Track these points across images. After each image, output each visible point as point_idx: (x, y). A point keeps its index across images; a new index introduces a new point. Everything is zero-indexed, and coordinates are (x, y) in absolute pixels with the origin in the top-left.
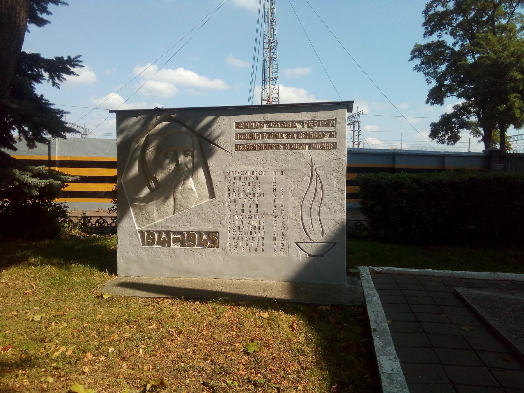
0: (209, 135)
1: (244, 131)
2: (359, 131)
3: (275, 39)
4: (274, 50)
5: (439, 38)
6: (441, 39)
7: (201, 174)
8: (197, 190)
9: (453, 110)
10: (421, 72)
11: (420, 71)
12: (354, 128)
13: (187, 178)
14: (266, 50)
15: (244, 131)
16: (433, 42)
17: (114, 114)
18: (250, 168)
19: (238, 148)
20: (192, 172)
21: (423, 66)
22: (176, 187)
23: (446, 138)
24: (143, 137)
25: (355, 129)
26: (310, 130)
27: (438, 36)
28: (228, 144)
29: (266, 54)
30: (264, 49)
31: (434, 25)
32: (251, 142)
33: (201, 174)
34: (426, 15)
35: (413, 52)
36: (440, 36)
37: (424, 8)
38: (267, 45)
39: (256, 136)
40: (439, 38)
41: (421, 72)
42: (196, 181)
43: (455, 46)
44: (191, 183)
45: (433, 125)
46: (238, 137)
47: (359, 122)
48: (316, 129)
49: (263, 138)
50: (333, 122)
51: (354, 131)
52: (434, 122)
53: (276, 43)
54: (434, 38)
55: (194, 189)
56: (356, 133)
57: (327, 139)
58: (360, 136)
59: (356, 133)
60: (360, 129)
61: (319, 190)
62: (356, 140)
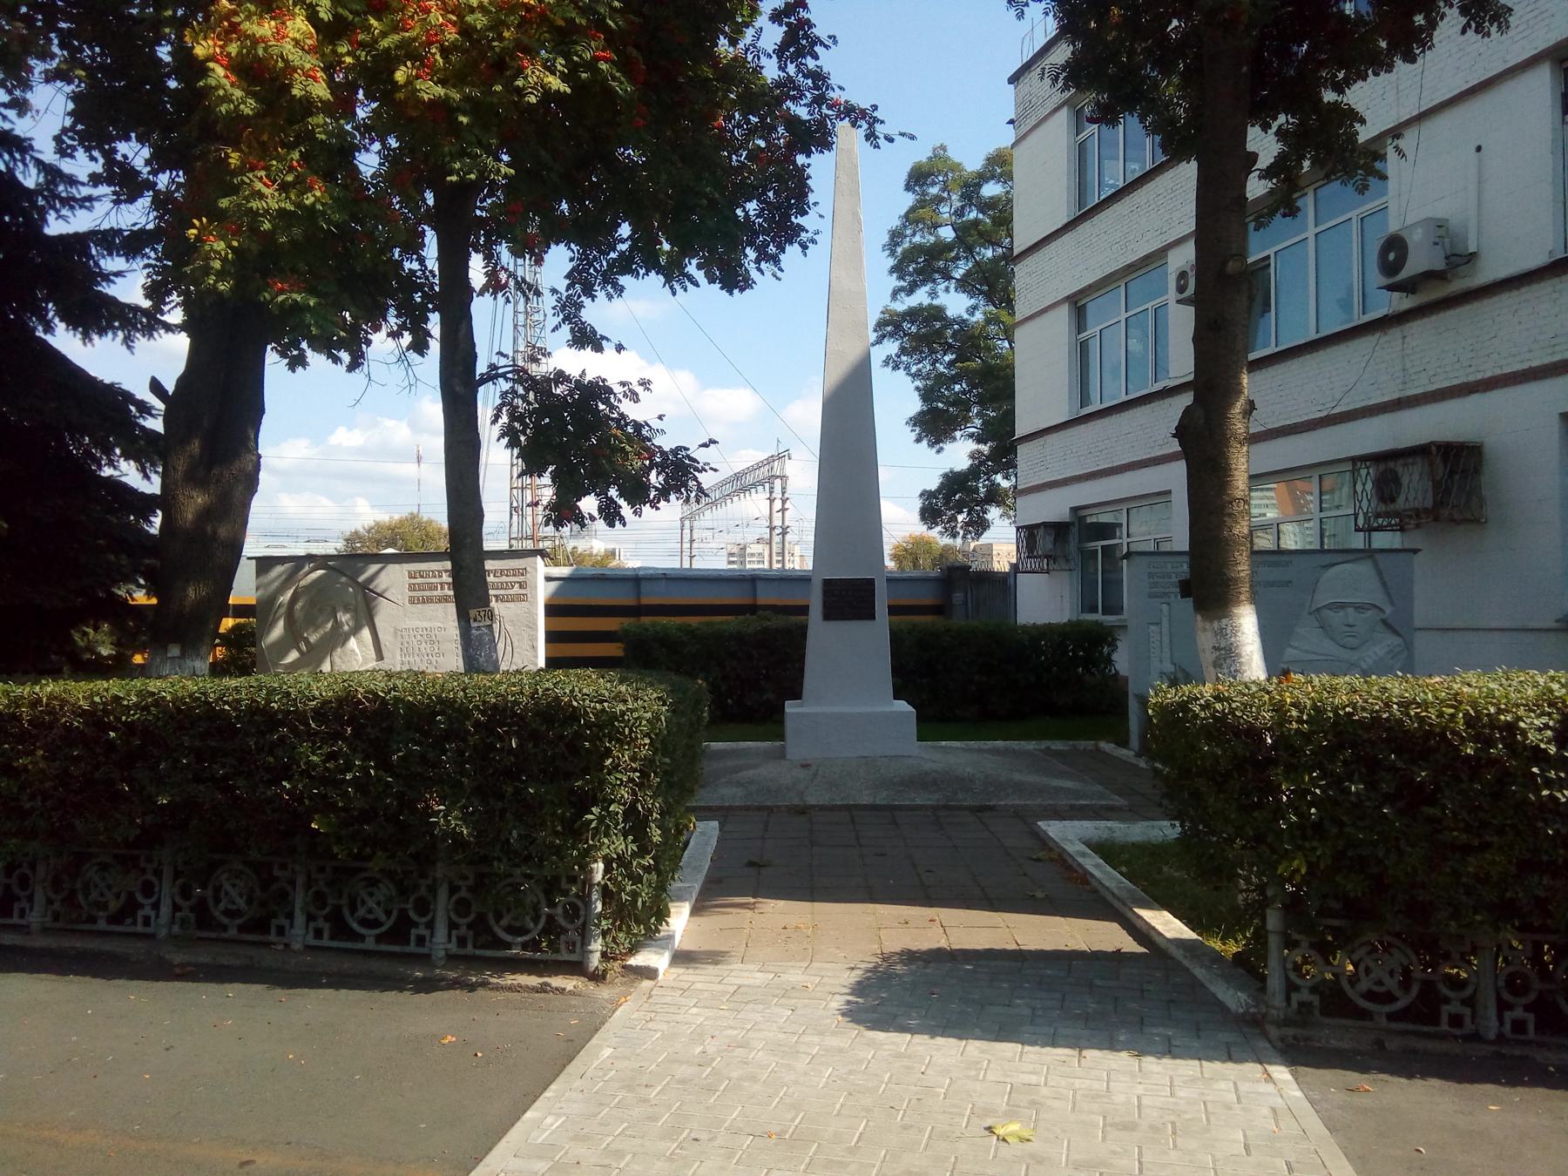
0: (375, 587)
1: (419, 580)
2: (784, 502)
3: (541, 306)
4: (538, 331)
5: (932, 298)
6: (936, 302)
7: (366, 633)
8: (361, 651)
9: (970, 462)
10: (902, 372)
11: (899, 368)
12: (771, 493)
13: (346, 640)
14: (520, 328)
15: (419, 580)
16: (921, 304)
17: (254, 561)
18: (426, 624)
19: (412, 601)
20: (355, 631)
21: (904, 358)
22: (333, 649)
23: (959, 525)
24: (290, 588)
25: (774, 495)
26: (496, 580)
27: (930, 294)
28: (399, 597)
29: (520, 339)
30: (515, 326)
31: (918, 272)
32: (428, 593)
33: (366, 633)
34: (893, 253)
35: (880, 325)
36: (933, 294)
37: (886, 238)
38: (521, 318)
39: (432, 587)
40: (932, 298)
41: (901, 370)
42: (360, 642)
43: (972, 314)
44: (352, 643)
45: (927, 495)
46: (412, 588)
47: (783, 478)
48: (504, 579)
49: (442, 589)
50: (523, 572)
51: (772, 501)
52: (928, 489)
53: (542, 316)
54: (921, 297)
55: (357, 651)
56: (778, 505)
57: (516, 590)
58: (787, 513)
59: (778, 505)
60: (786, 496)
61: (509, 649)
62: (777, 522)
